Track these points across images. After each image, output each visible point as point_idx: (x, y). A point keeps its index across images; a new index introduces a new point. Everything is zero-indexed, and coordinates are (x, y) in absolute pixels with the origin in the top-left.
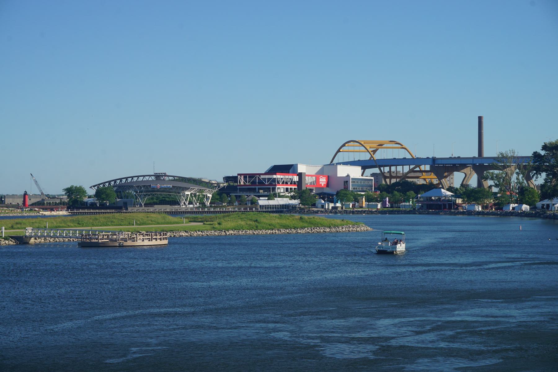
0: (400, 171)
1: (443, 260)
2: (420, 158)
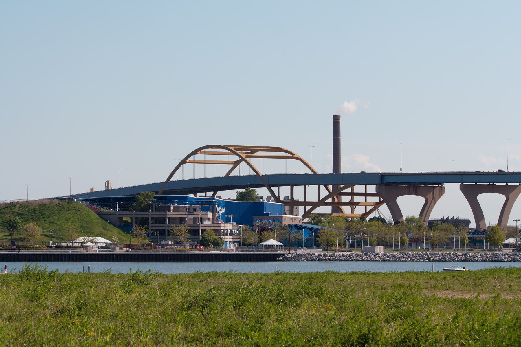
0: (288, 197)
1: (109, 253)
2: (235, 176)
